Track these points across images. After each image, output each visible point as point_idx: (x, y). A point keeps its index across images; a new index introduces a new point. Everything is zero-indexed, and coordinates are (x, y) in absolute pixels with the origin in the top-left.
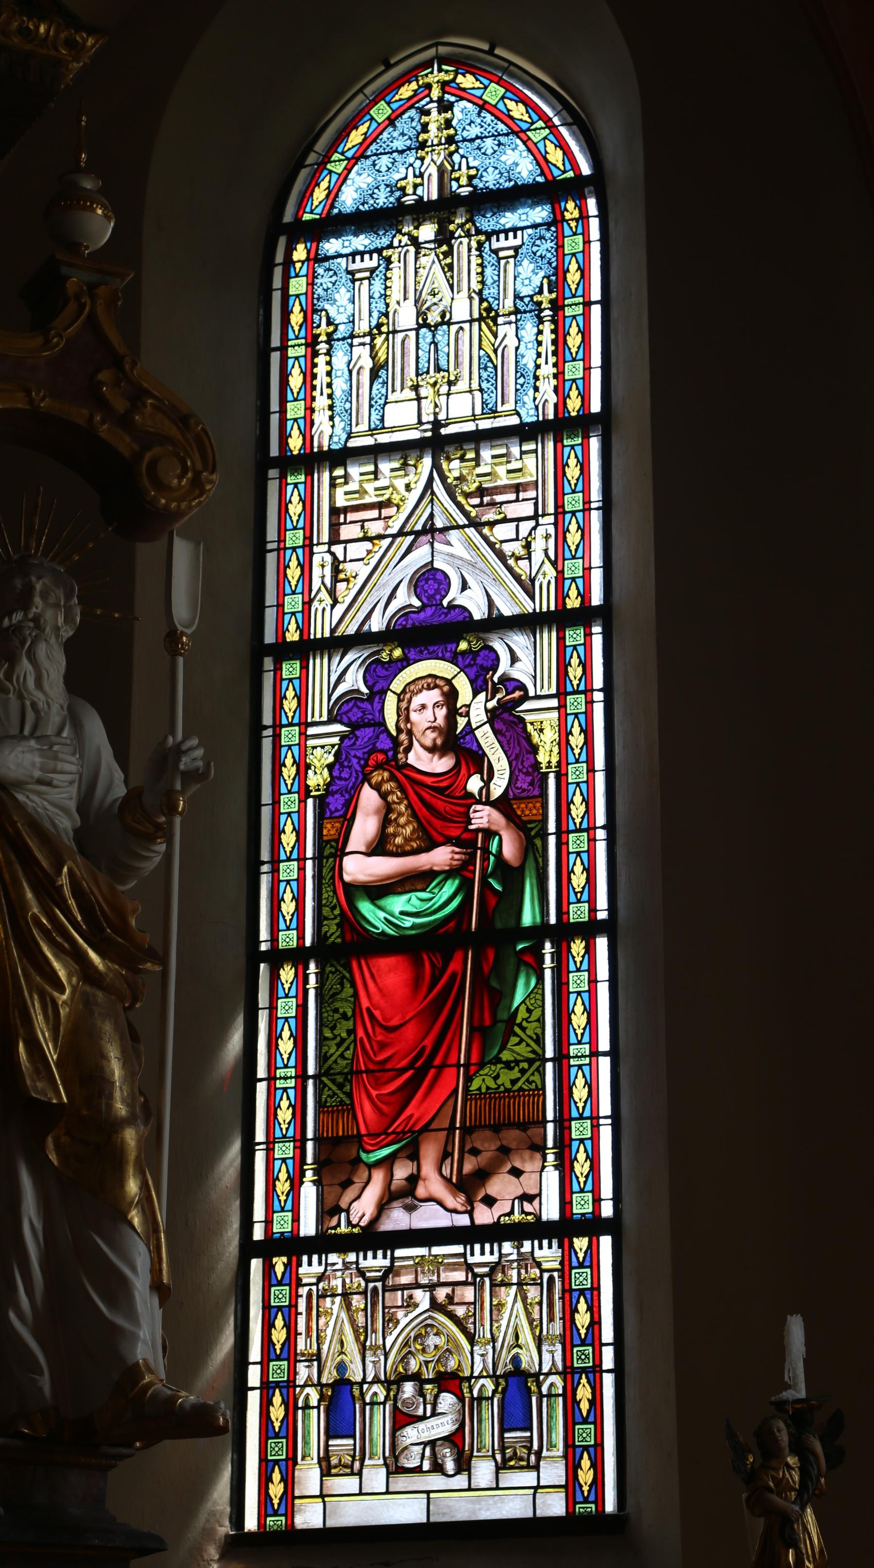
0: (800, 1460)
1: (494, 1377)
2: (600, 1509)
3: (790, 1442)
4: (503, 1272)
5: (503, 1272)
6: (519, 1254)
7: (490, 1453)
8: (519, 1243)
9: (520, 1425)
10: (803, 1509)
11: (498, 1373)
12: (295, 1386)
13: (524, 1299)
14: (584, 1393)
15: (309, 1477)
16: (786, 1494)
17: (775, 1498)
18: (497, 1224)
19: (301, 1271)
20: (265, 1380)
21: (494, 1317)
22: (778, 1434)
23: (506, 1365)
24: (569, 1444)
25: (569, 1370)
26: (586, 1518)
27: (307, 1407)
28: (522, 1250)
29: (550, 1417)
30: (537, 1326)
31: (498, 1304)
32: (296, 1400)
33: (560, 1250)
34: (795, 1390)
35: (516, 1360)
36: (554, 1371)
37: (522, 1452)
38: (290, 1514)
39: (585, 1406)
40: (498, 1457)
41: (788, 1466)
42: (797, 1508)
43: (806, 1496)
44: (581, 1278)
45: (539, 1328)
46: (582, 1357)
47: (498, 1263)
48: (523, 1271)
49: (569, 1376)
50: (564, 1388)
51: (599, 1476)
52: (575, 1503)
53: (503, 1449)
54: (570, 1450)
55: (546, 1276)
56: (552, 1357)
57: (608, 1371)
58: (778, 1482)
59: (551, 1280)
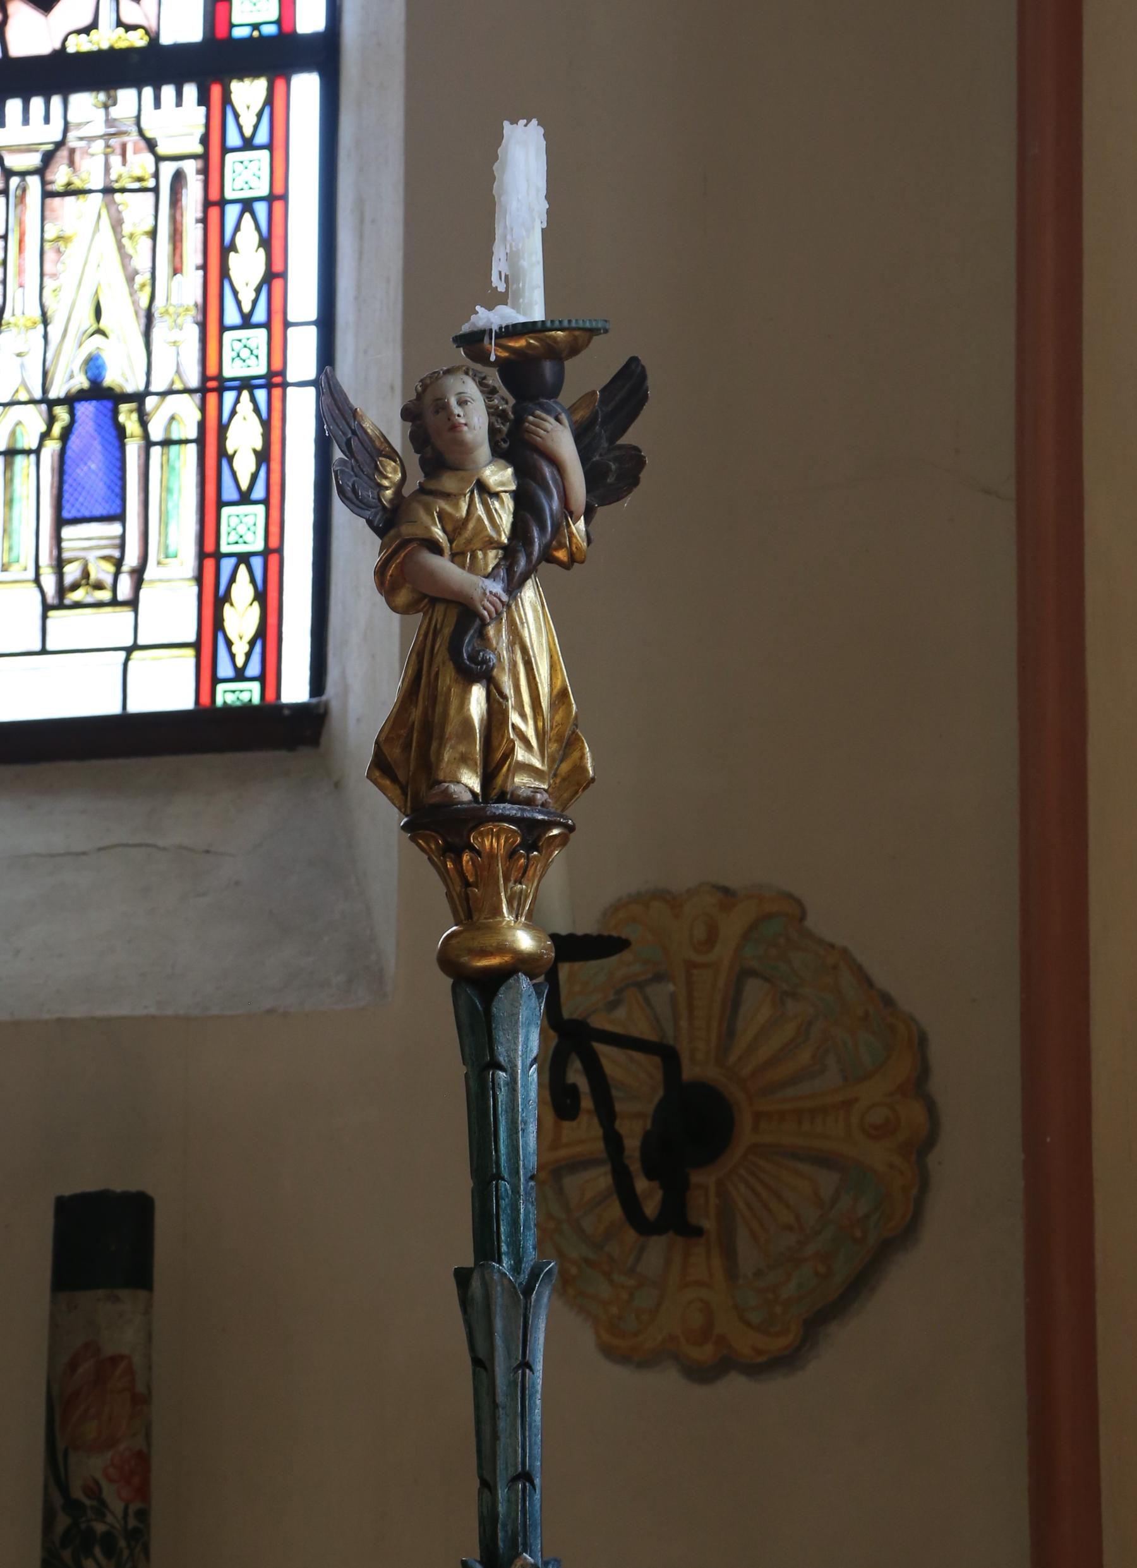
0: (517, 474)
2: (270, 695)
3: (492, 431)
4: (71, 163)
5: (71, 163)
6: (109, 122)
7: (31, 574)
8: (109, 97)
9: (98, 511)
10: (514, 587)
13: (117, 224)
14: (244, 436)
16: (474, 557)
17: (443, 565)
18: (60, 54)
21: (48, 268)
22: (457, 410)
23: (71, 377)
24: (208, 553)
25: (212, 384)
28: (114, 112)
29: (166, 489)
30: (143, 286)
31: (59, 238)
33: (203, 109)
34: (516, 307)
35: (93, 365)
36: (178, 386)
37: (102, 571)
39: (245, 466)
40: (49, 582)
41: (482, 488)
42: (496, 587)
43: (522, 562)
44: (246, 175)
45: (148, 289)
46: (244, 355)
48: (116, 160)
49: (212, 398)
50: (202, 425)
51: (272, 620)
52: (215, 681)
53: (59, 565)
54: (209, 564)
55: (168, 170)
56: (178, 354)
58: (454, 529)
59: (179, 178)
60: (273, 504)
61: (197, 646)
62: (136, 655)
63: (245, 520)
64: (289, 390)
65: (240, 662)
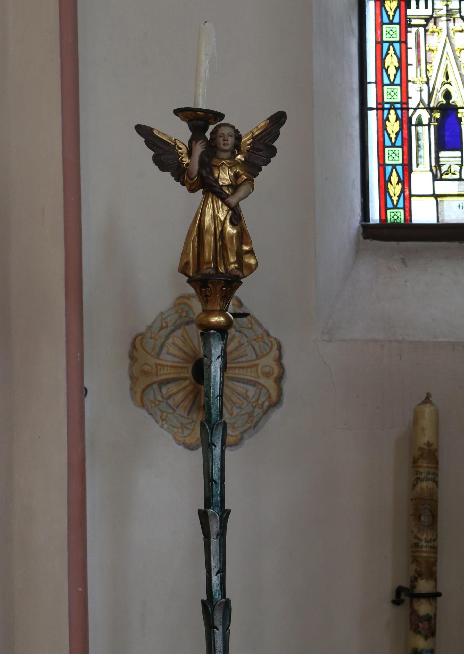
1: (431, 110)
11: (432, 105)
12: (408, 109)
15: (421, 180)
19: (410, 12)
20: (380, 101)
26: (396, 226)
27: (420, 123)
32: (410, 119)
38: (408, 210)
47: (432, 16)
57: (372, 109)
60: (379, 43)
61: (408, 81)
62: (433, 199)
63: (391, 154)
64: (375, 107)
65: (395, 203)
